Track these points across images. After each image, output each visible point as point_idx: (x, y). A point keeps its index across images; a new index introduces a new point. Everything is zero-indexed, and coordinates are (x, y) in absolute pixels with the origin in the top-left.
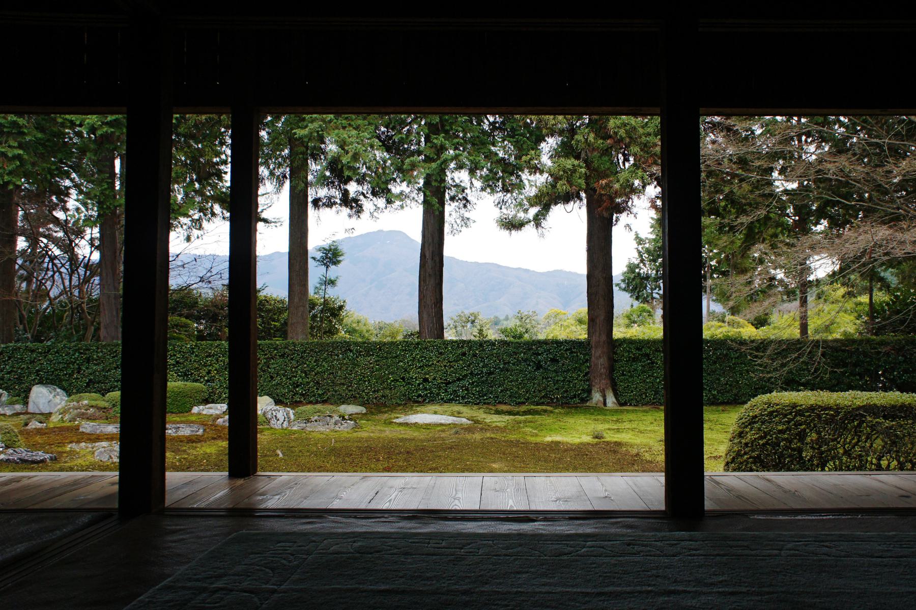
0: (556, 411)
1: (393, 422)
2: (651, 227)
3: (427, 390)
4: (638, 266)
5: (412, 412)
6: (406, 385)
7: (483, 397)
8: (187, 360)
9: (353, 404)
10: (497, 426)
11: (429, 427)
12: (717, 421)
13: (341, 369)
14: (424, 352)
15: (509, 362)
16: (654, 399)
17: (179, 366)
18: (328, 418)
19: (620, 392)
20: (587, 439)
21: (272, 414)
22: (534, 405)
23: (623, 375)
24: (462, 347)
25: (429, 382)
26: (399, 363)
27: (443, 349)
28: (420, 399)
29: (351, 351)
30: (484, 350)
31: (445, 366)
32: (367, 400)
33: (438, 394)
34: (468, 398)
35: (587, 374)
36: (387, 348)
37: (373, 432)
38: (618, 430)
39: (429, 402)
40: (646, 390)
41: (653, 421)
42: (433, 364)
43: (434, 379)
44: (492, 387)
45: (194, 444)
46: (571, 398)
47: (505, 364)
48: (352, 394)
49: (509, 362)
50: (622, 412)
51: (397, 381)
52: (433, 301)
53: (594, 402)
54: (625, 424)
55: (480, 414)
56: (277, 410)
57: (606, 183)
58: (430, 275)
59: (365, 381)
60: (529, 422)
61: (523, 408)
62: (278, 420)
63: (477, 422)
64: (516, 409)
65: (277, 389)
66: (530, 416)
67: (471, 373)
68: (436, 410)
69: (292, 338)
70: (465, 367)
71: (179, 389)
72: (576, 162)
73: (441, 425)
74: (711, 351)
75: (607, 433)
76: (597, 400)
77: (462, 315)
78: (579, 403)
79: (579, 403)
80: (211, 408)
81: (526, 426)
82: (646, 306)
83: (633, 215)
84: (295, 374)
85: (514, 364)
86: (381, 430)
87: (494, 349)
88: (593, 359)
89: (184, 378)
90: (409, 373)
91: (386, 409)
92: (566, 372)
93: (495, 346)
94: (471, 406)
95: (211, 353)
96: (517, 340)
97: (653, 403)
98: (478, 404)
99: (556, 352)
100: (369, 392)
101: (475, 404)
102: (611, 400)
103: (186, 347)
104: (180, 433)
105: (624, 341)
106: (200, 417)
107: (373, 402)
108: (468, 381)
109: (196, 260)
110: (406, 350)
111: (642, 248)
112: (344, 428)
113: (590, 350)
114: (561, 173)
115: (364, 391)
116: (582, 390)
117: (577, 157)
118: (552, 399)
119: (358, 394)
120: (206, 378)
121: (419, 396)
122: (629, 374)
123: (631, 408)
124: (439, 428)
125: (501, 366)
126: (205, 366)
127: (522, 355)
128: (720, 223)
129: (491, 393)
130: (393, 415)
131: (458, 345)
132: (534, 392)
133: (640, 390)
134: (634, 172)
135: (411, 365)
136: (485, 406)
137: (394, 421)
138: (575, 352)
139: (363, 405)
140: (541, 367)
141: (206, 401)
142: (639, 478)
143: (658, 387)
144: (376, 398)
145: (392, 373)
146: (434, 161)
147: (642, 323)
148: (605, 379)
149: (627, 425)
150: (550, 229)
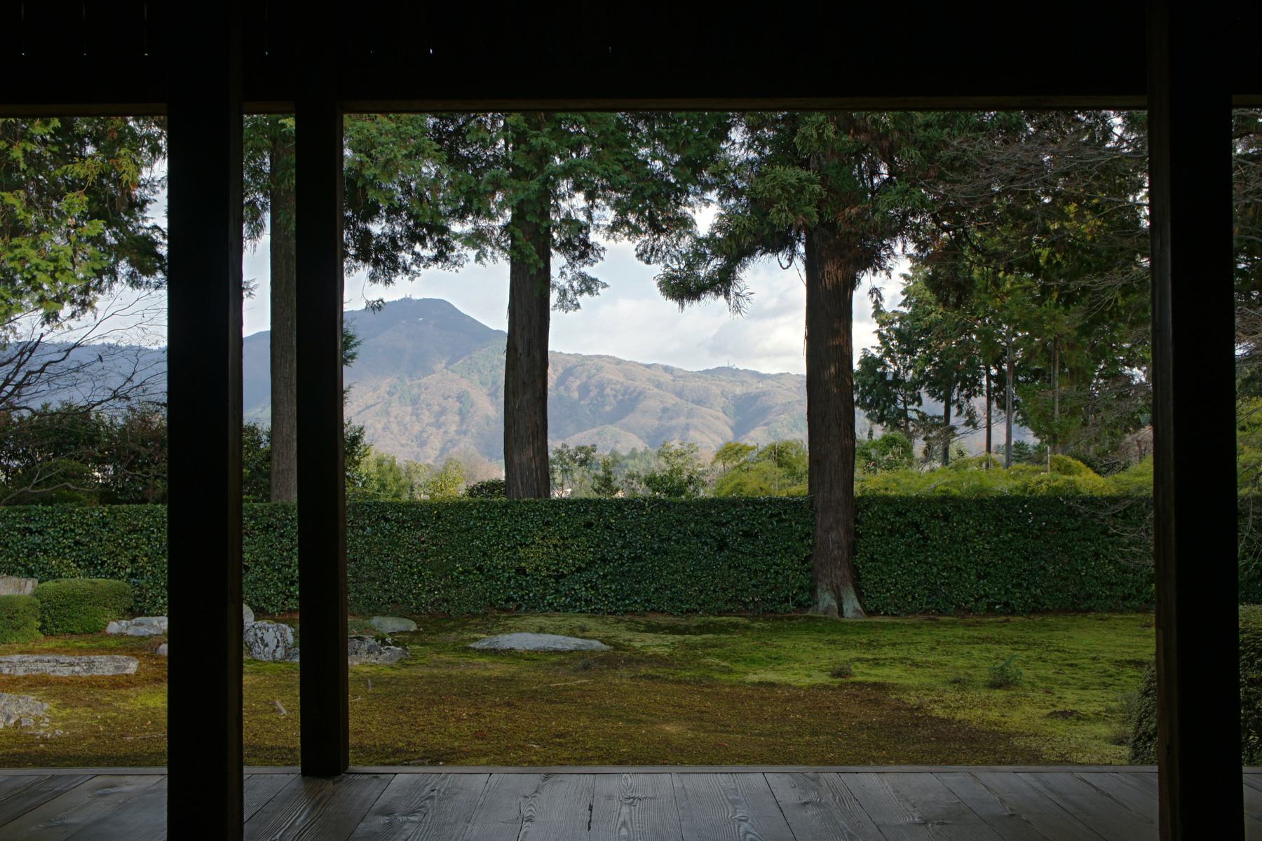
0: (756, 625)
1: (470, 648)
2: (903, 293)
3: (523, 589)
4: (880, 362)
5: (501, 629)
6: (486, 580)
7: (624, 600)
8: (94, 539)
9: (391, 616)
10: (655, 655)
11: (535, 656)
12: (1050, 644)
13: (369, 552)
14: (516, 522)
15: (669, 539)
16: (928, 603)
17: (80, 550)
18: (357, 641)
19: (867, 591)
20: (822, 679)
21: (256, 635)
22: (714, 615)
23: (872, 560)
24: (586, 511)
25: (527, 576)
26: (472, 541)
27: (551, 515)
28: (511, 605)
29: (387, 520)
30: (624, 517)
31: (555, 546)
32: (417, 609)
33: (543, 597)
34: (597, 603)
35: (808, 559)
36: (451, 514)
37: (436, 667)
38: (876, 663)
39: (526, 611)
40: (913, 587)
41: (934, 644)
42: (533, 543)
43: (536, 569)
44: (639, 582)
45: (123, 691)
46: (781, 603)
47: (662, 541)
48: (390, 597)
49: (669, 539)
50: (873, 626)
51: (470, 572)
52: (529, 432)
53: (821, 609)
54: (885, 649)
55: (623, 635)
56: (265, 628)
57: (857, 214)
58: (524, 383)
59: (413, 574)
60: (711, 647)
61: (696, 620)
62: (267, 645)
63: (617, 647)
64: (683, 622)
65: (256, 588)
66: (710, 636)
67: (603, 559)
68: (543, 625)
69: (278, 497)
70: (590, 547)
71: (85, 590)
72: (804, 174)
73: (557, 652)
74: (1030, 517)
75: (856, 667)
76: (826, 605)
77: (565, 450)
78: (794, 611)
79: (794, 611)
80: (141, 624)
81: (709, 654)
82: (897, 434)
83: (884, 272)
84: (287, 562)
85: (677, 542)
86: (452, 663)
87: (643, 516)
88: (819, 532)
89: (89, 571)
90: (491, 558)
91: (452, 623)
92: (770, 555)
93: (644, 509)
94: (602, 618)
95: (137, 525)
96: (673, 499)
97: (926, 612)
98: (614, 613)
99: (754, 520)
100: (420, 594)
101: (609, 613)
102: (851, 604)
103: (92, 516)
104: (97, 672)
105: (870, 500)
106: (123, 640)
107: (426, 610)
108: (596, 572)
109: (101, 359)
110: (485, 518)
111: (888, 331)
112: (386, 659)
113: (813, 515)
114: (778, 191)
115: (410, 591)
116: (801, 588)
117: (805, 164)
118: (745, 604)
119: (401, 596)
120: (128, 570)
121: (509, 599)
122: (883, 559)
123: (887, 620)
124: (553, 659)
125: (656, 546)
126: (127, 549)
127: (693, 525)
128: (1043, 286)
129: (638, 594)
130: (466, 636)
131: (578, 508)
132: (714, 591)
133: (903, 587)
134: (907, 191)
135: (494, 545)
136: (627, 618)
137: (472, 645)
138: (785, 520)
139: (409, 615)
140: (726, 545)
141: (132, 613)
142: (1047, 776)
143: (936, 583)
144: (432, 604)
145: (461, 559)
146: (528, 175)
147: (891, 466)
148: (840, 568)
149: (889, 653)
150: (749, 296)
